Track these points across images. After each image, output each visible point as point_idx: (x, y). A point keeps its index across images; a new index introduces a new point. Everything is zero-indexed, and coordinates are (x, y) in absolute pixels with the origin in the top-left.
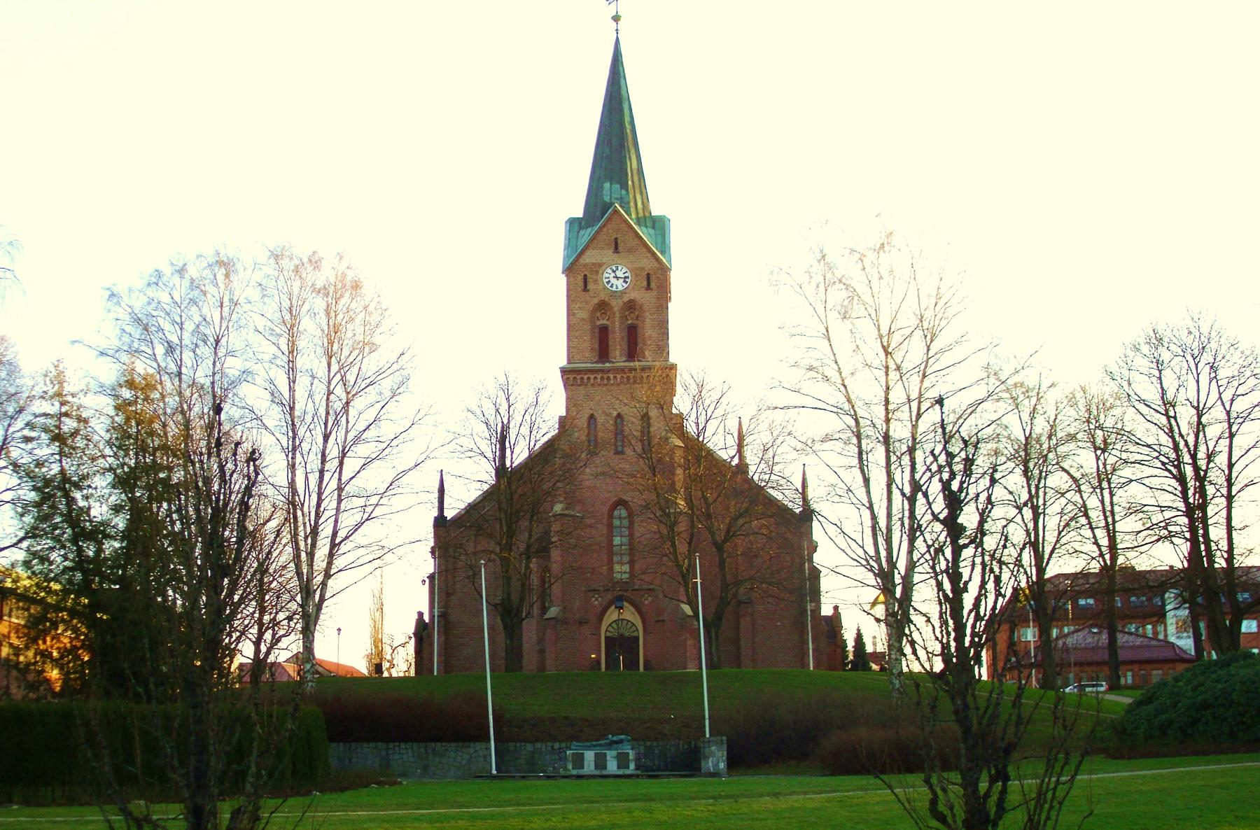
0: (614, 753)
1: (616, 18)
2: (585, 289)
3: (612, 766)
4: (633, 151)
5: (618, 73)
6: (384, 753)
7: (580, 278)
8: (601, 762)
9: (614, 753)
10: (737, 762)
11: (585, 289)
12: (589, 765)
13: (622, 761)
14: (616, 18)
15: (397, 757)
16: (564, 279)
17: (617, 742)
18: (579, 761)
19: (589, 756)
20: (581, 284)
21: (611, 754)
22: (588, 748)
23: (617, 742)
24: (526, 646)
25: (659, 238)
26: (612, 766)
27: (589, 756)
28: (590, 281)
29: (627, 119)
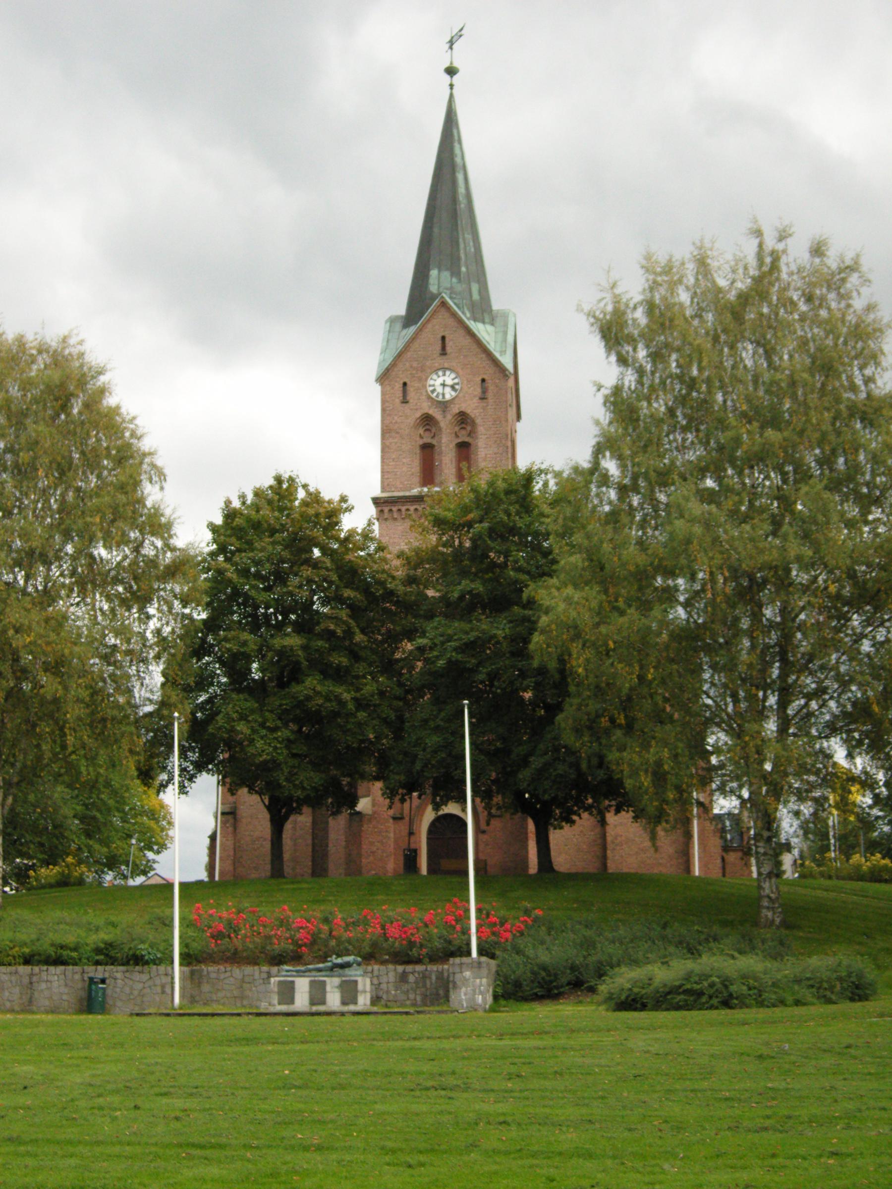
0: (336, 981)
1: (451, 71)
2: (405, 401)
3: (334, 1000)
4: (468, 237)
5: (452, 135)
6: (26, 980)
7: (398, 386)
8: (318, 994)
9: (336, 981)
10: (511, 991)
11: (405, 401)
12: (301, 1001)
13: (349, 992)
14: (451, 71)
15: (43, 986)
16: (378, 388)
17: (343, 966)
18: (287, 992)
19: (302, 985)
20: (399, 394)
21: (332, 984)
22: (301, 974)
23: (343, 966)
24: (332, 849)
25: (500, 335)
26: (334, 1000)
27: (302, 985)
28: (411, 390)
29: (461, 190)
